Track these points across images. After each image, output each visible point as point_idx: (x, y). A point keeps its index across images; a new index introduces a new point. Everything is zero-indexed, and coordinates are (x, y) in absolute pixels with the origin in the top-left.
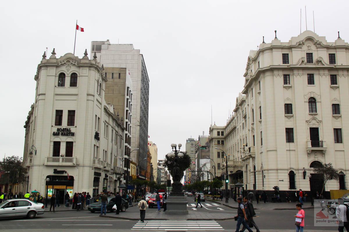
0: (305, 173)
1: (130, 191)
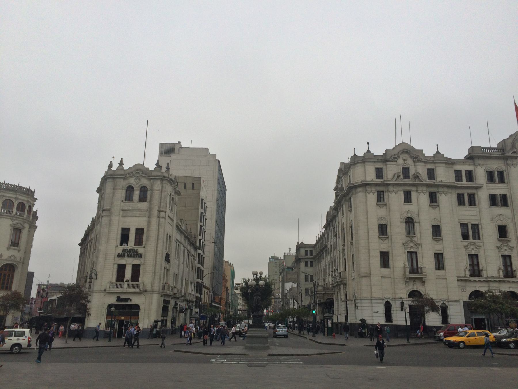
0: (402, 304)
1: (203, 322)
